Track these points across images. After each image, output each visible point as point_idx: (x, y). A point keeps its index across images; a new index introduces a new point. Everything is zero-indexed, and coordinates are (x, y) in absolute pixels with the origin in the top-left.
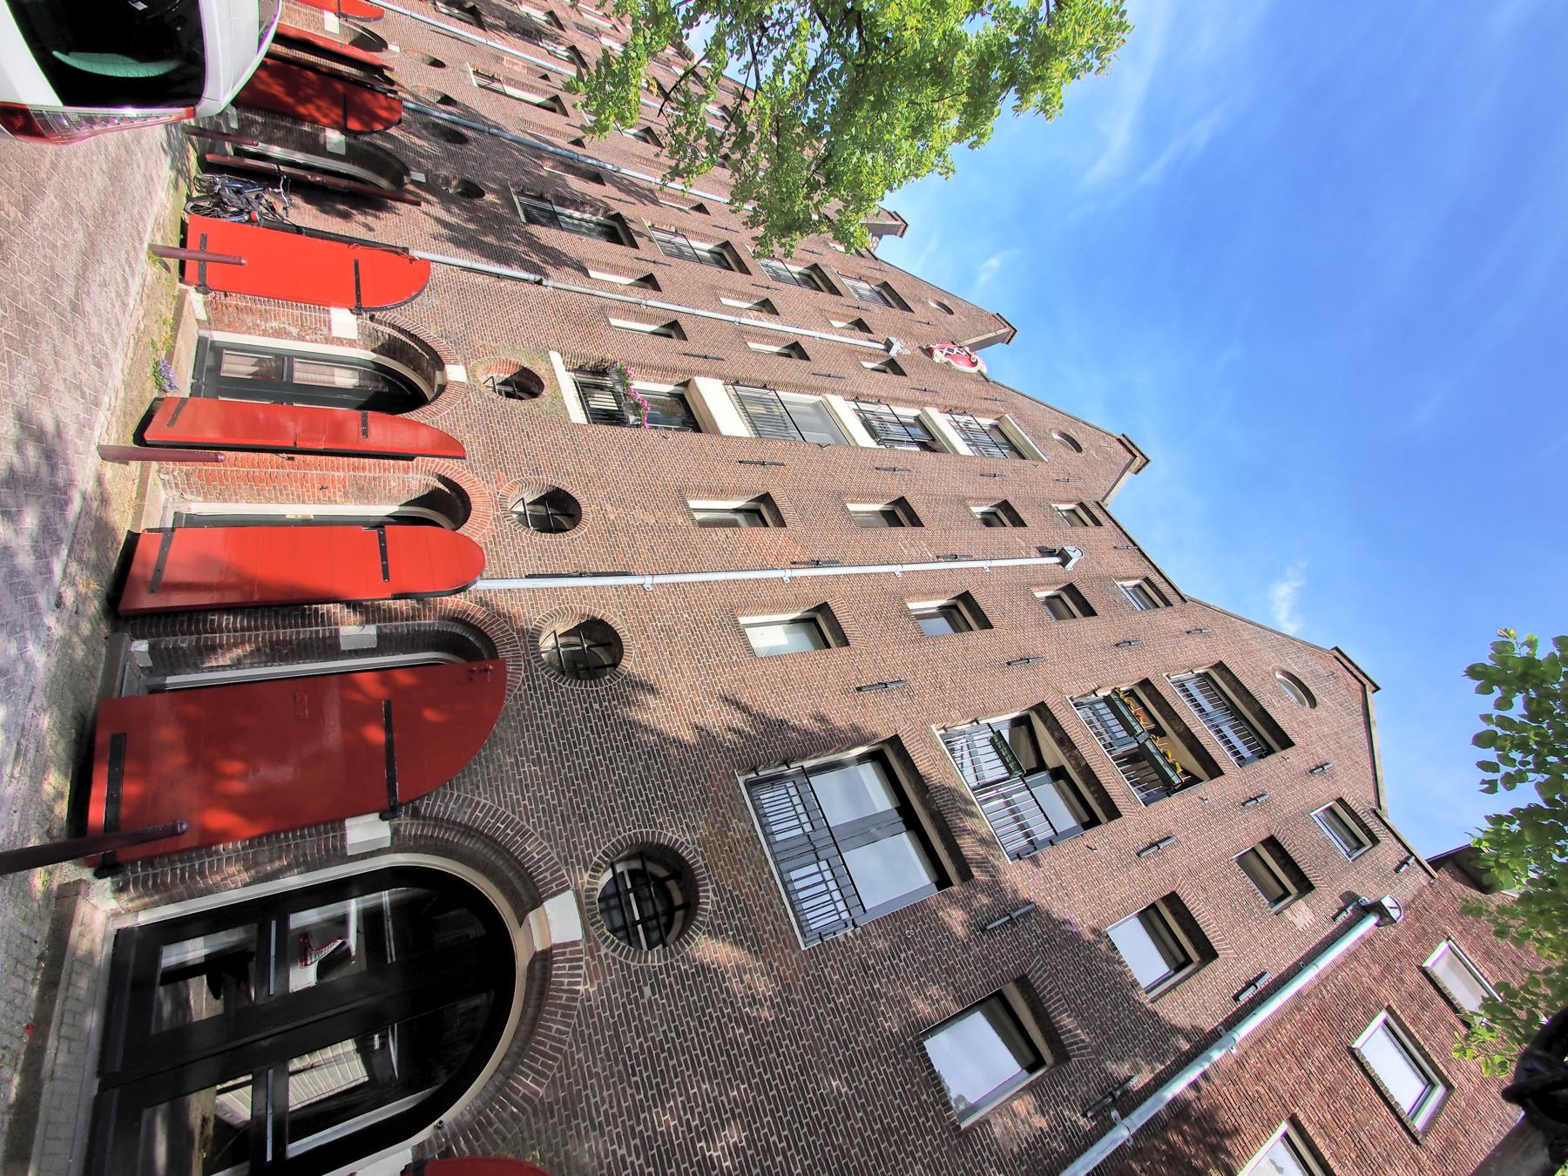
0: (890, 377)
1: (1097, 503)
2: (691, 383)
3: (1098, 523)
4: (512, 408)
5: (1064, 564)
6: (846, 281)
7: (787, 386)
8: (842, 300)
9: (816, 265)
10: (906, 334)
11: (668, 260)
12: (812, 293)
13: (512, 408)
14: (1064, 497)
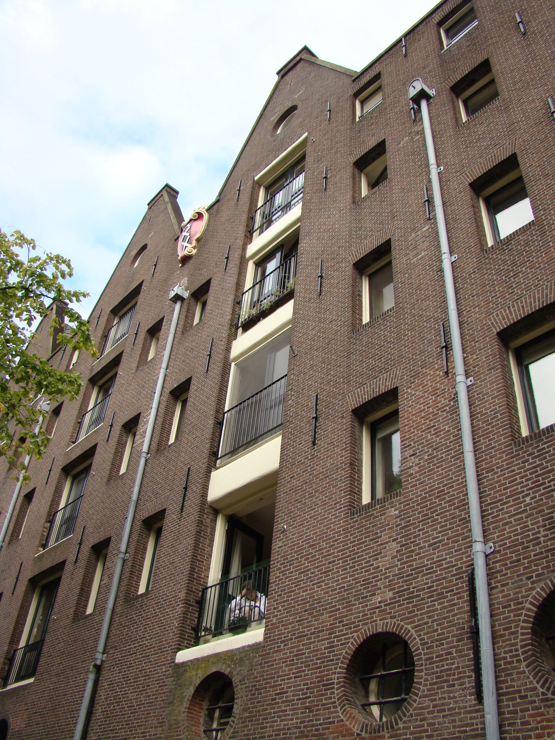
0: (211, 297)
1: (353, 81)
2: (215, 506)
3: (378, 77)
4: (245, 710)
5: (428, 97)
6: (82, 437)
7: (221, 400)
8: (127, 350)
9: (112, 311)
10: (167, 284)
11: (79, 530)
12: (118, 381)
13: (245, 710)
14: (349, 112)
